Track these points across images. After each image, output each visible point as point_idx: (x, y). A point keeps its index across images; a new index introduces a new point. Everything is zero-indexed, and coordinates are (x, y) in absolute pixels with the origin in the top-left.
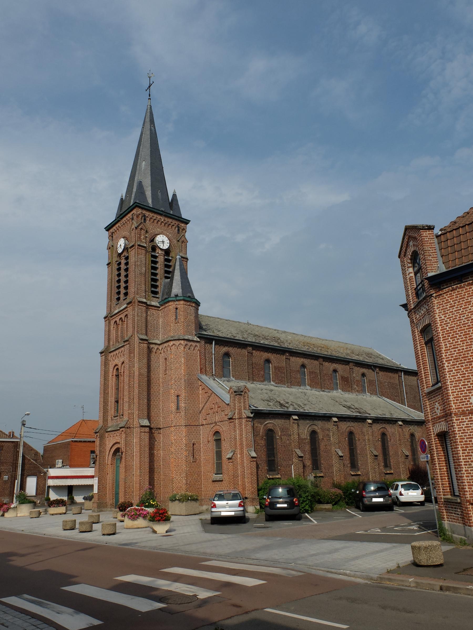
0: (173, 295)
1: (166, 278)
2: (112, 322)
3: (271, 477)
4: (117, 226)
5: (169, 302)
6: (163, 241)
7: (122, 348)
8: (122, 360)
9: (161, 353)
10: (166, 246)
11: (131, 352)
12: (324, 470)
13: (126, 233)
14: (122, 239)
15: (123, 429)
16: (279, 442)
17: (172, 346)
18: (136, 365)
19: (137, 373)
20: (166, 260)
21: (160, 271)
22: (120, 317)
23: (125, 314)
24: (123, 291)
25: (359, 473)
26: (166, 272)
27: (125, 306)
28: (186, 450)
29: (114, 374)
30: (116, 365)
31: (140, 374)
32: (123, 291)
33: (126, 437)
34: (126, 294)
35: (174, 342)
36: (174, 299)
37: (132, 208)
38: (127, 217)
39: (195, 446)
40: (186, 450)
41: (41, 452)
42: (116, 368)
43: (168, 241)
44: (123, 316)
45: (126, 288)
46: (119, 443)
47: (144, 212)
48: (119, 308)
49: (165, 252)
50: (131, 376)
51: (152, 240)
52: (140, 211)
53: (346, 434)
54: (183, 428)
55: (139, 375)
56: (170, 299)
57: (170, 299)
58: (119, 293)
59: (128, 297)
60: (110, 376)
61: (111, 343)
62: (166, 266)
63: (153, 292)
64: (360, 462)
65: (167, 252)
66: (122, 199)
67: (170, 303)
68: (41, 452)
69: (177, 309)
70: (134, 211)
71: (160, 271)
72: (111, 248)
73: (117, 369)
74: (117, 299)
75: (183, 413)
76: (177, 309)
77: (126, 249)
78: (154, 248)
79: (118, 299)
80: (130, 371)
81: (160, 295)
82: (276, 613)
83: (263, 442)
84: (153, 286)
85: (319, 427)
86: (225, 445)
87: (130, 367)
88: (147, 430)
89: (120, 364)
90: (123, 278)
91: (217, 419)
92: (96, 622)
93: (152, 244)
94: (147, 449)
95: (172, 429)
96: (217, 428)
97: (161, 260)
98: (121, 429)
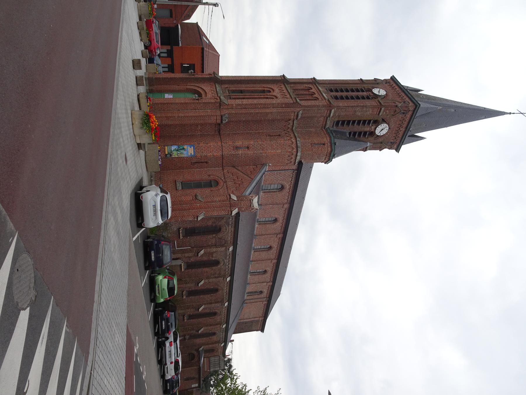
0: (336, 140)
1: (350, 133)
2: (311, 86)
3: (181, 231)
4: (396, 87)
5: (330, 137)
6: (382, 130)
7: (289, 96)
8: (278, 95)
9: (284, 130)
10: (378, 132)
11: (287, 105)
12: (187, 271)
13: (390, 96)
14: (385, 93)
15: (219, 100)
16: (211, 236)
17: (292, 141)
18: (275, 110)
19: (268, 111)
20: (365, 133)
21: (357, 128)
22: (316, 93)
23: (319, 97)
24: (339, 94)
25: (184, 297)
26: (355, 133)
27: (326, 97)
28: (201, 156)
29: (265, 89)
30: (273, 90)
31: (267, 114)
32: (339, 94)
33: (212, 103)
34: (336, 98)
35: (295, 143)
36: (333, 142)
37: (413, 100)
38: (405, 97)
39: (205, 164)
40: (201, 156)
41: (193, 20)
42: (271, 90)
43: (382, 134)
44: (316, 95)
45: (342, 98)
46: (206, 96)
47: (410, 113)
48: (324, 91)
49: (372, 132)
50: (265, 106)
51: (384, 121)
52: (411, 109)
53: (216, 287)
54: (220, 154)
55: (266, 113)
56: (332, 138)
57: (332, 138)
58: (337, 91)
59: (334, 100)
60: (263, 85)
61: (292, 85)
62: (360, 133)
63: (338, 122)
64: (193, 297)
65: (372, 133)
66: (420, 90)
67: (328, 139)
68: (193, 20)
69: (324, 144)
70: (411, 104)
71: (357, 128)
72: (376, 82)
73: (270, 92)
74: (337, 96)
75: (233, 152)
76: (324, 144)
77: (376, 96)
78: (377, 123)
79: (331, 91)
80: (270, 104)
81: (335, 128)
82: (61, 337)
83: (210, 223)
84: (343, 122)
85: (223, 267)
86: (207, 191)
87: (273, 104)
88: (219, 121)
89: (275, 94)
90: (350, 94)
91: (230, 184)
92: (29, 308)
93: (380, 120)
94: (202, 122)
95: (219, 144)
96: (221, 183)
97: (367, 129)
98: (218, 98)
